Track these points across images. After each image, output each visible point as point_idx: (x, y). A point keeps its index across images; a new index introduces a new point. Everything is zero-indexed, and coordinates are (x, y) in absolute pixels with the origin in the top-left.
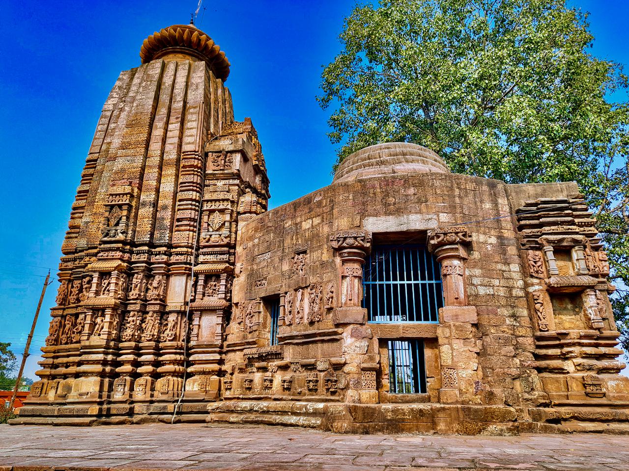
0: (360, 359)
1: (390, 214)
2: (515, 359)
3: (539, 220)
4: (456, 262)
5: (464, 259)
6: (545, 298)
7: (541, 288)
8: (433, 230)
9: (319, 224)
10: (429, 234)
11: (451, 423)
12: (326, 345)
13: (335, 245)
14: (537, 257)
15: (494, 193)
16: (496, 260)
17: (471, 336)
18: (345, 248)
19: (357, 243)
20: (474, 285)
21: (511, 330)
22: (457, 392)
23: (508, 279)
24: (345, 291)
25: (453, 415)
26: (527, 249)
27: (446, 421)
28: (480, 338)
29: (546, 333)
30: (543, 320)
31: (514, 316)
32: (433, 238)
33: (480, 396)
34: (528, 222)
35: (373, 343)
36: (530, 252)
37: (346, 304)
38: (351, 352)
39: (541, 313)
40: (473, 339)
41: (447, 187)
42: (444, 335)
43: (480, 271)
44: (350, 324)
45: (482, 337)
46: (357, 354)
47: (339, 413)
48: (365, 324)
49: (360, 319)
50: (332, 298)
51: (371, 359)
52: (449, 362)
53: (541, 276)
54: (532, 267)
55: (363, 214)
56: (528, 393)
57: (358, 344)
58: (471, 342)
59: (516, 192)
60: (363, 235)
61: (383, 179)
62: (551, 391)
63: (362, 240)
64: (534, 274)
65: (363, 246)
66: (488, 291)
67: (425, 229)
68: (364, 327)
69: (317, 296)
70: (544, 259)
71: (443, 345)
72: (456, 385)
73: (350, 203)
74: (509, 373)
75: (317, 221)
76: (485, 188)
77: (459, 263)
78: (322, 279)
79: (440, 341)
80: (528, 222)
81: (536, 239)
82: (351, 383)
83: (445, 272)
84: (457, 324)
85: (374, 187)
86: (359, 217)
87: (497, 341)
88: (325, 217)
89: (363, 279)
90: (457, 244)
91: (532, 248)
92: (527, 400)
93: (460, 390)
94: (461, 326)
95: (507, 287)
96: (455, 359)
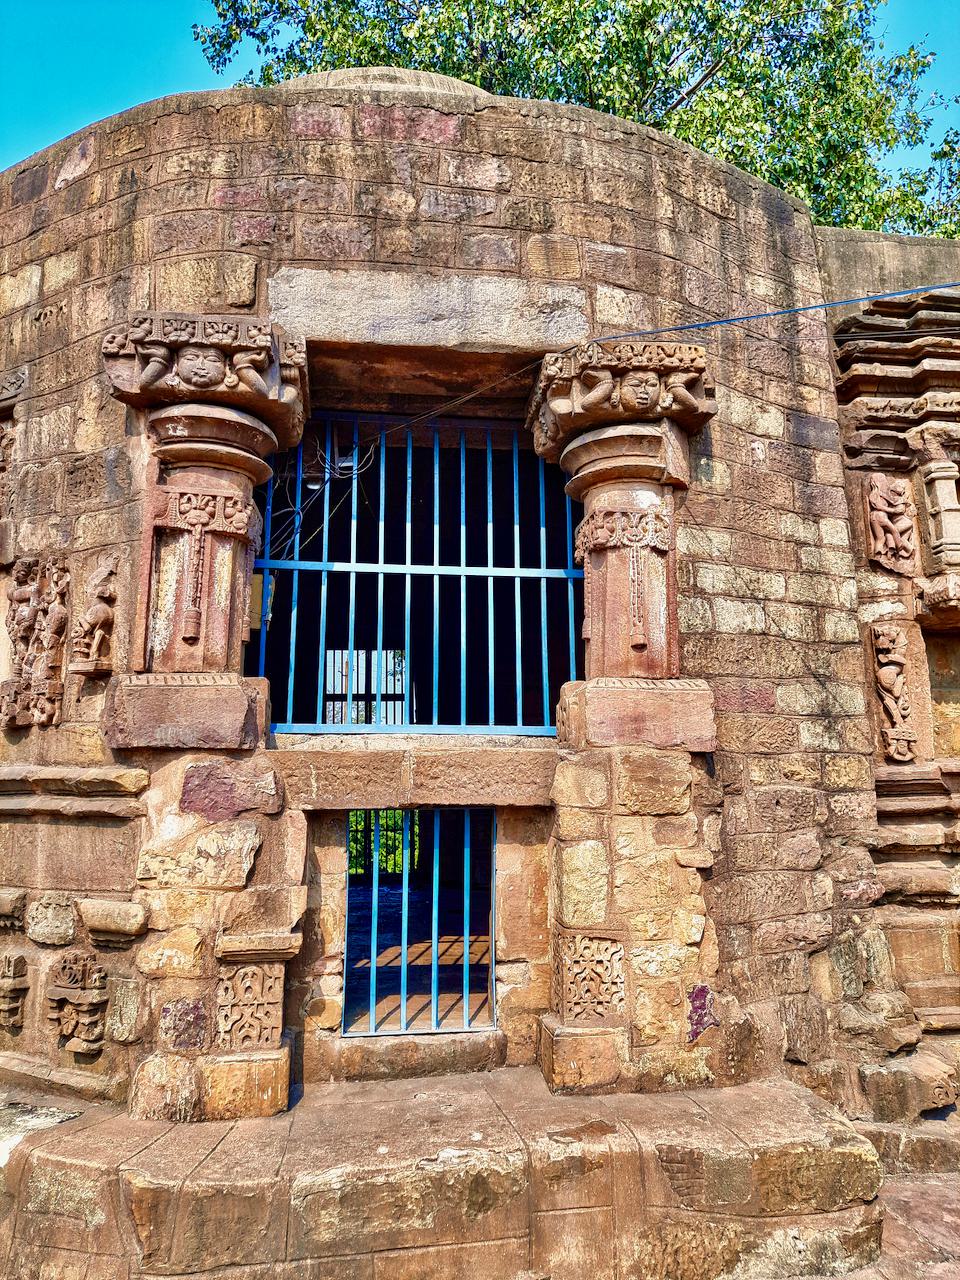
0: (216, 910)
1: (392, 264)
2: (820, 876)
3: (913, 363)
4: (646, 498)
5: (677, 487)
6: (909, 645)
7: (900, 608)
8: (567, 352)
9: (70, 285)
10: (552, 370)
11: (609, 1231)
12: (69, 835)
13: (130, 377)
14: (901, 500)
15: (784, 243)
16: (778, 500)
17: (686, 801)
18: (175, 398)
19: (231, 379)
20: (700, 592)
21: (812, 766)
22: (621, 1039)
23: (812, 573)
24: (171, 598)
25: (619, 1191)
26: (867, 468)
27: (588, 1225)
28: (716, 809)
29: (907, 769)
30: (901, 726)
31: (825, 715)
32: (564, 391)
33: (707, 1051)
34: (878, 370)
35: (280, 835)
36: (879, 478)
37: (167, 656)
38: (178, 878)
39: (897, 699)
40: (692, 816)
41: (629, 178)
42: (582, 798)
43: (727, 537)
44: (179, 751)
45: (721, 805)
46: (203, 889)
47: (77, 1214)
48: (250, 752)
49: (228, 725)
50: (108, 625)
51: (268, 907)
52: (598, 913)
53: (905, 566)
54: (880, 532)
55: (271, 251)
56: (855, 1000)
57: (210, 842)
58: (683, 827)
59: (843, 258)
60: (263, 341)
61: (367, 99)
62: (911, 975)
63: (258, 367)
64: (882, 560)
65: (261, 395)
66: (748, 618)
67: (538, 347)
68: (247, 764)
69: (45, 612)
70: (921, 506)
71: (578, 840)
72: (621, 1008)
73: (215, 192)
74: (799, 934)
75: (62, 270)
76: (756, 215)
77: (657, 500)
78: (69, 535)
79: (568, 821)
80: (878, 370)
81: (901, 435)
82: (165, 1023)
83: (602, 536)
84: (638, 752)
85: (325, 134)
86: (248, 264)
87: (768, 813)
88: (96, 256)
89: (259, 552)
90: (656, 421)
91: (886, 466)
92: (855, 1033)
93: (634, 1030)
94: (653, 764)
95: (809, 605)
96: (621, 900)
